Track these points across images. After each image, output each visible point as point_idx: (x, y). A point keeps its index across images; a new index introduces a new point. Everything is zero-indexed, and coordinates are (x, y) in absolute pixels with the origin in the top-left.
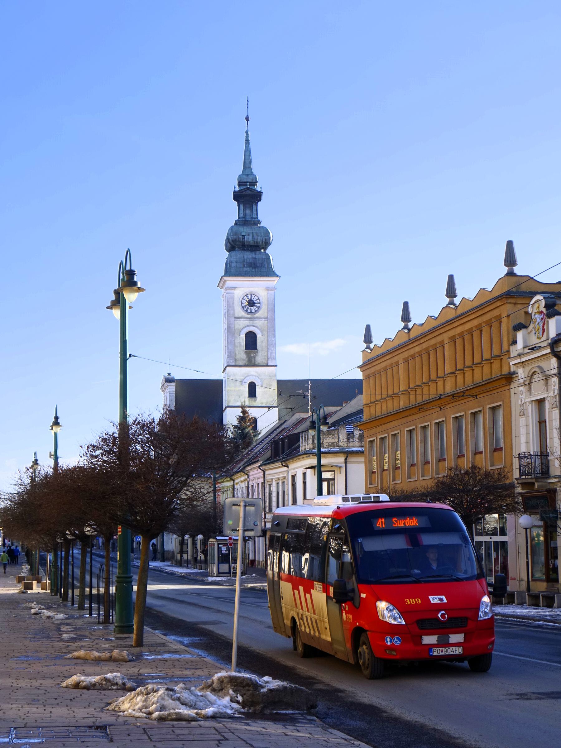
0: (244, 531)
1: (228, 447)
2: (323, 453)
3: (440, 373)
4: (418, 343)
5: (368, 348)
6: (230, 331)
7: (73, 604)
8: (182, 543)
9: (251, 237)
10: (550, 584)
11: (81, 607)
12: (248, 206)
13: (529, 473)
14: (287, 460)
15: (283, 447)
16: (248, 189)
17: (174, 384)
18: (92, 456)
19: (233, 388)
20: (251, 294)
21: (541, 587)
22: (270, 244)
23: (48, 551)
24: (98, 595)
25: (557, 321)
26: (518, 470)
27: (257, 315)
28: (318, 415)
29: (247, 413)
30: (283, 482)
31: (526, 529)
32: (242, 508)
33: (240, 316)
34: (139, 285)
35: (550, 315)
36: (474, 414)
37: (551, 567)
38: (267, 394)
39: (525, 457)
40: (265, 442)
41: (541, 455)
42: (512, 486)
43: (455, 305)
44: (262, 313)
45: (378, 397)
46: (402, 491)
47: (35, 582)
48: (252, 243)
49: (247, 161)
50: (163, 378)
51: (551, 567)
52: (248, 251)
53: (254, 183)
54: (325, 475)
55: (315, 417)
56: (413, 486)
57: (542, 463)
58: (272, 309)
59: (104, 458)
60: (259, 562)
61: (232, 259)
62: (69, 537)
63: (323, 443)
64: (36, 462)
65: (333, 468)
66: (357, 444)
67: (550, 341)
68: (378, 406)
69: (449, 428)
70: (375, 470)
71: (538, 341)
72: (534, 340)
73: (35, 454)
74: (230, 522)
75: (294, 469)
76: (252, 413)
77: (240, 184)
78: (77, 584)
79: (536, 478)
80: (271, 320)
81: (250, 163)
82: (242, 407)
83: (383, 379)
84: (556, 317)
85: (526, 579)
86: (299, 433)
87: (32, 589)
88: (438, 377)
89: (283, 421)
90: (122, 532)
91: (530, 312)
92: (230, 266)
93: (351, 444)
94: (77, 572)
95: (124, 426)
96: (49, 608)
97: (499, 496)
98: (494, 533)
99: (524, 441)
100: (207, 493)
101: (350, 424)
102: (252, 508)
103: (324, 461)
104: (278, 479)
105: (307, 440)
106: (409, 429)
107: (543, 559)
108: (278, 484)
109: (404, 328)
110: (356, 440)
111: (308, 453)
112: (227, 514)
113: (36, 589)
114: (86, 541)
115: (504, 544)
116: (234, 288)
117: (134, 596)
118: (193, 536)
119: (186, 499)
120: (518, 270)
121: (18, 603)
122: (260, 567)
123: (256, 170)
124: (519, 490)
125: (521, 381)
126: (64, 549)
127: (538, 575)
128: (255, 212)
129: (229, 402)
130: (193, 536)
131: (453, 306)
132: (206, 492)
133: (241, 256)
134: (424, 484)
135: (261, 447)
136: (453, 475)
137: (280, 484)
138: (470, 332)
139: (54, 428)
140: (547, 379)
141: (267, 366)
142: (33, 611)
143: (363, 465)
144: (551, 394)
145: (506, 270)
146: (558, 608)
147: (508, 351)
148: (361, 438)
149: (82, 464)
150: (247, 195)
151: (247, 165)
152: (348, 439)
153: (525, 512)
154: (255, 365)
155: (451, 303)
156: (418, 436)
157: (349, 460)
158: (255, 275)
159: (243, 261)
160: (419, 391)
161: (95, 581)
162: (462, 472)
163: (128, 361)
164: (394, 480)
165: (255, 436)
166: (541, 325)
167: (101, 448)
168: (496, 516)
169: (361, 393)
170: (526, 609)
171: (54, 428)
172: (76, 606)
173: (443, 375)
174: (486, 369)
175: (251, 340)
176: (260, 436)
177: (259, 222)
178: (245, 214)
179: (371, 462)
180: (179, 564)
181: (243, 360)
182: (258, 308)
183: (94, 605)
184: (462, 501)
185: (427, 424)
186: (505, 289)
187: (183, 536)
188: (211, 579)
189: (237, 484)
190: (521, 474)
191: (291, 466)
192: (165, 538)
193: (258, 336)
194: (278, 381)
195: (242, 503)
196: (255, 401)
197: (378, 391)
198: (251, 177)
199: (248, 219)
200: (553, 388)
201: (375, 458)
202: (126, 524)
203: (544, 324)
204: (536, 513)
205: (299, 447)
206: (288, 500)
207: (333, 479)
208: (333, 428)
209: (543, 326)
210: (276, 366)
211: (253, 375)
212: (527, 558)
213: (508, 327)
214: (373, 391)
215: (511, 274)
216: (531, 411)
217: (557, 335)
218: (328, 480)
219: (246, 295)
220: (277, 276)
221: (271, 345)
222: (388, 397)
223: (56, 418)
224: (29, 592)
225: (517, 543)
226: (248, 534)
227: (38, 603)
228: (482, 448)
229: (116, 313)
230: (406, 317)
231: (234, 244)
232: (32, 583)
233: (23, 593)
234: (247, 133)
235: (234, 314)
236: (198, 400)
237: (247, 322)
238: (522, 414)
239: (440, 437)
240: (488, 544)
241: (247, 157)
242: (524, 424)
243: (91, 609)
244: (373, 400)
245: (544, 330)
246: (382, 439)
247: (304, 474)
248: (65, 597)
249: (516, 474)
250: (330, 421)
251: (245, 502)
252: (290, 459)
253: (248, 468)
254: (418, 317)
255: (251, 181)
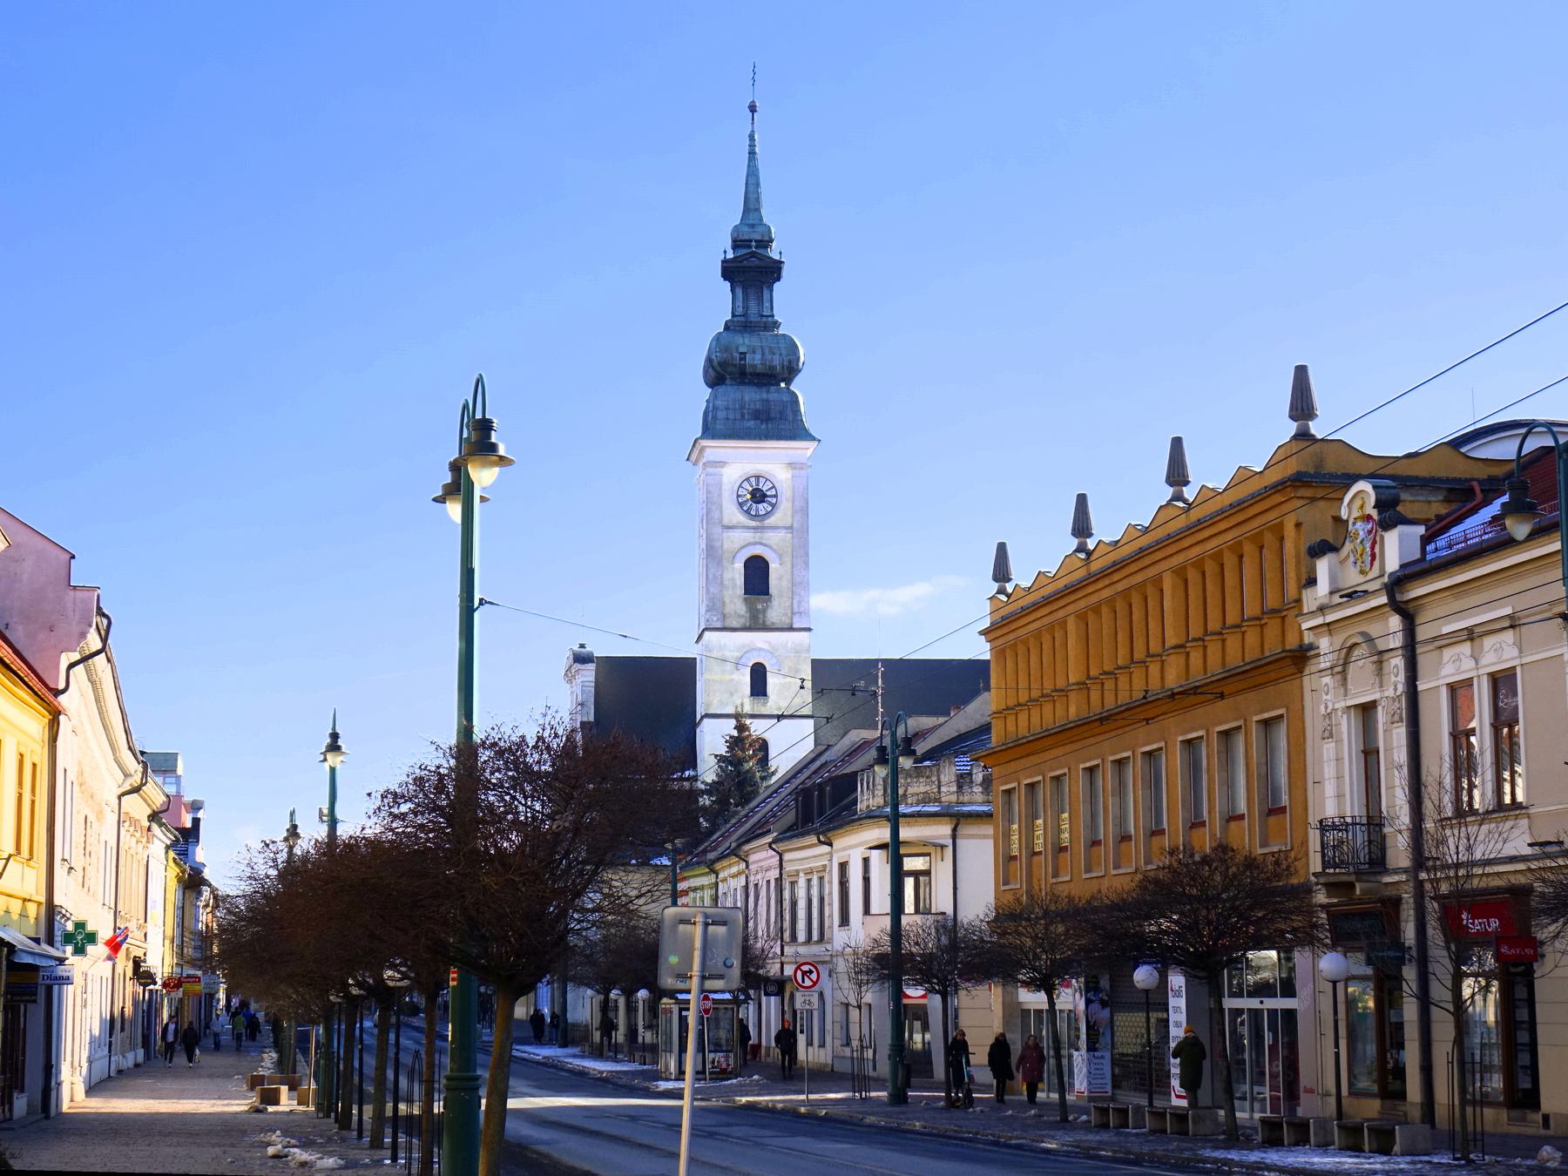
0: (703, 978)
1: (705, 801)
2: (905, 815)
3: (1155, 646)
4: (1107, 581)
5: (1001, 591)
6: (713, 554)
7: (360, 1136)
8: (606, 1007)
9: (758, 356)
10: (1388, 1103)
11: (376, 1144)
12: (751, 291)
13: (1342, 862)
14: (829, 830)
15: (822, 803)
16: (753, 255)
17: (592, 666)
18: (395, 817)
19: (716, 677)
20: (758, 477)
21: (1371, 1108)
22: (799, 371)
23: (314, 1022)
24: (410, 1117)
25: (1400, 536)
26: (1319, 856)
27: (771, 521)
28: (894, 734)
29: (748, 729)
30: (821, 878)
31: (1334, 983)
32: (699, 930)
33: (734, 522)
34: (502, 451)
35: (1386, 525)
36: (1226, 734)
37: (1390, 1066)
38: (787, 689)
39: (1334, 827)
40: (784, 792)
41: (1369, 824)
42: (1307, 890)
43: (1185, 501)
44: (781, 516)
45: (1023, 697)
46: (1070, 898)
47: (284, 1089)
48: (760, 369)
49: (752, 197)
50: (569, 654)
51: (1390, 1066)
52: (752, 386)
53: (766, 243)
54: (910, 864)
55: (887, 742)
56: (1093, 887)
57: (1370, 842)
58: (803, 511)
59: (420, 820)
60: (768, 1048)
61: (719, 403)
62: (355, 991)
63: (905, 795)
64: (293, 832)
65: (927, 848)
66: (979, 798)
67: (1386, 579)
68: (1023, 717)
69: (1174, 763)
70: (1015, 852)
71: (1361, 579)
72: (1352, 578)
73: (292, 814)
74: (673, 960)
75: (844, 849)
76: (757, 728)
77: (736, 244)
78: (370, 1089)
79: (1358, 873)
80: (799, 531)
81: (758, 200)
82: (737, 716)
83: (1034, 659)
84: (1400, 528)
85: (1333, 1091)
86: (855, 773)
87: (277, 1103)
88: (1149, 655)
89: (822, 748)
90: (460, 980)
91: (1345, 517)
92: (715, 418)
93: (966, 798)
94: (370, 1061)
95: (466, 749)
96: (305, 1145)
97: (1276, 911)
98: (1263, 990)
99: (1333, 793)
100: (638, 897)
101: (964, 753)
102: (722, 930)
103: (905, 833)
104: (810, 872)
105: (871, 789)
106: (1088, 765)
107: (1371, 1049)
108: (809, 881)
109: (1078, 550)
110: (978, 789)
111: (872, 816)
112: (666, 943)
113: (287, 1102)
114: (384, 996)
115: (1290, 1015)
116: (722, 464)
117: (482, 1117)
118: (629, 993)
119: (593, 911)
120: (1317, 429)
121: (244, 1133)
122: (770, 1060)
123: (770, 216)
124: (1321, 897)
125: (1324, 663)
126: (343, 1017)
127: (1364, 1083)
128: (767, 304)
129: (708, 705)
130: (629, 993)
131: (1181, 504)
132: (635, 893)
133: (738, 396)
134: (1118, 884)
135: (775, 802)
136: (1175, 865)
137: (815, 882)
138: (1218, 557)
139: (329, 756)
140: (1380, 656)
141: (791, 629)
142: (271, 1151)
143: (991, 842)
144: (1390, 693)
145: (1292, 428)
146: (1402, 1155)
147: (1299, 601)
148: (987, 783)
149: (369, 833)
150: (751, 269)
151: (752, 205)
152: (960, 787)
153: (1333, 947)
154: (766, 628)
155: (1178, 497)
156: (1107, 779)
157: (962, 831)
158: (767, 436)
159: (742, 407)
160: (1109, 684)
161: (403, 1082)
162: (1197, 858)
163: (476, 615)
164: (1056, 875)
165: (763, 778)
166: (1368, 545)
167: (410, 800)
168: (1273, 954)
169: (987, 688)
170: (1334, 1156)
171: (329, 756)
172: (367, 1140)
173: (1160, 650)
174: (1252, 638)
175: (757, 575)
176: (774, 779)
177: (776, 325)
178: (746, 307)
179: (1007, 835)
180: (598, 1053)
181: (740, 616)
182: (773, 506)
183: (402, 1139)
184: (1196, 922)
185: (1125, 755)
186: (1291, 468)
187: (607, 993)
188: (663, 1085)
189: (725, 880)
190: (1325, 865)
191: (837, 844)
192: (569, 996)
193: (772, 566)
194: (813, 661)
195: (699, 919)
196: (765, 704)
197: (1023, 684)
198: (760, 229)
199: (754, 318)
200: (1393, 679)
201: (1015, 827)
202: (468, 965)
203: (1374, 543)
204: (1360, 949)
205: (855, 802)
206: (831, 916)
207: (927, 873)
208: (927, 763)
209: (1373, 548)
210: (809, 630)
211: (761, 649)
212: (1337, 1046)
213: (1297, 548)
214: (1012, 684)
215: (1303, 436)
216: (1347, 727)
217: (1402, 566)
218: (916, 874)
219: (747, 479)
220: (814, 439)
221: (799, 586)
222: (1043, 696)
223: (335, 736)
224: (271, 1109)
225: (1317, 1012)
226: (709, 984)
227: (285, 1133)
228: (1242, 807)
229: (454, 510)
230: (1082, 527)
231: (724, 371)
232: (277, 1091)
233: (258, 1111)
234: (752, 137)
235: (721, 520)
236: (644, 701)
237: (749, 536)
238: (1329, 734)
239: (1153, 782)
240: (1255, 1014)
241: (751, 188)
242: (1333, 756)
243: (395, 1146)
244: (1011, 703)
245: (1373, 556)
246: (1032, 786)
247: (866, 861)
248: (344, 1121)
249: (1316, 864)
250: (921, 748)
251: (706, 916)
252: (835, 828)
253: (746, 847)
254: (1107, 529)
255: (758, 237)
